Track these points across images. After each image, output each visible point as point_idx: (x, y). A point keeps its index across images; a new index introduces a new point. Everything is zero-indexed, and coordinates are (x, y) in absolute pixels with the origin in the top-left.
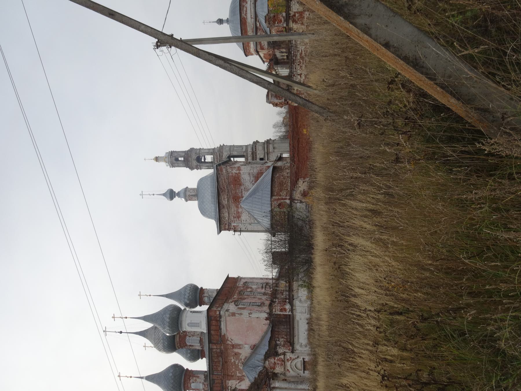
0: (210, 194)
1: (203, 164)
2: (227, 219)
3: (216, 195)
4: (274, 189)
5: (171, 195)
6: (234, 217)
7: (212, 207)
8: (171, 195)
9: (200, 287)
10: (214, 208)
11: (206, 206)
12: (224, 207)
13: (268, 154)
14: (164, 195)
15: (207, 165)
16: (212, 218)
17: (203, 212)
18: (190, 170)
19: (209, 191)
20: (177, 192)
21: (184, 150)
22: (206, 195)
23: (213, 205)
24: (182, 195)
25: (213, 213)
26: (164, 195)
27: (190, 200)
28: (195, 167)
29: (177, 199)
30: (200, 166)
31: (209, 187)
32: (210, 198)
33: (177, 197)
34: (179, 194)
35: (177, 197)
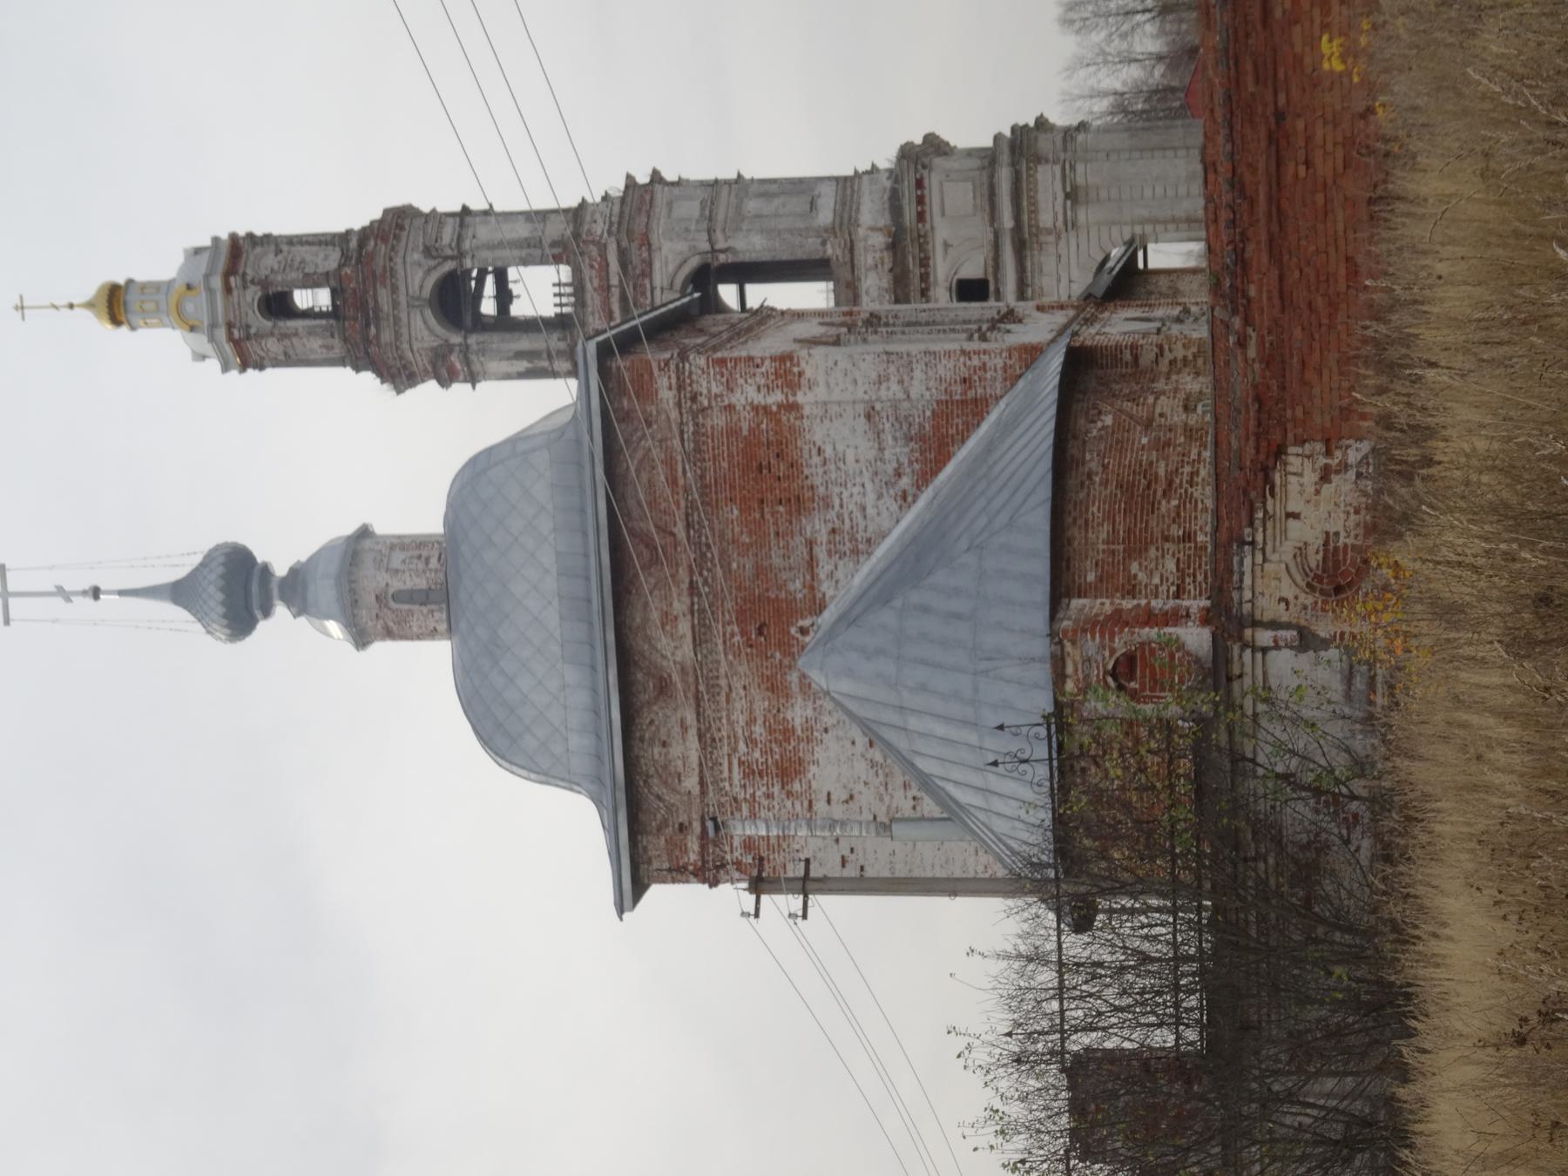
0: (550, 584)
1: (495, 340)
2: (691, 783)
4: (642, 817)
5: (236, 591)
6: (750, 772)
8: (236, 591)
9: (259, 560)
10: (581, 698)
12: (664, 688)
13: (1020, 247)
14: (180, 592)
15: (525, 343)
16: (567, 781)
17: (500, 728)
18: (386, 390)
19: (547, 558)
20: (280, 570)
23: (572, 675)
24: (324, 590)
25: (579, 742)
26: (180, 592)
27: (389, 634)
28: (421, 362)
29: (280, 627)
30: (465, 350)
31: (545, 525)
32: (552, 617)
33: (281, 611)
34: (296, 588)
35: (281, 611)
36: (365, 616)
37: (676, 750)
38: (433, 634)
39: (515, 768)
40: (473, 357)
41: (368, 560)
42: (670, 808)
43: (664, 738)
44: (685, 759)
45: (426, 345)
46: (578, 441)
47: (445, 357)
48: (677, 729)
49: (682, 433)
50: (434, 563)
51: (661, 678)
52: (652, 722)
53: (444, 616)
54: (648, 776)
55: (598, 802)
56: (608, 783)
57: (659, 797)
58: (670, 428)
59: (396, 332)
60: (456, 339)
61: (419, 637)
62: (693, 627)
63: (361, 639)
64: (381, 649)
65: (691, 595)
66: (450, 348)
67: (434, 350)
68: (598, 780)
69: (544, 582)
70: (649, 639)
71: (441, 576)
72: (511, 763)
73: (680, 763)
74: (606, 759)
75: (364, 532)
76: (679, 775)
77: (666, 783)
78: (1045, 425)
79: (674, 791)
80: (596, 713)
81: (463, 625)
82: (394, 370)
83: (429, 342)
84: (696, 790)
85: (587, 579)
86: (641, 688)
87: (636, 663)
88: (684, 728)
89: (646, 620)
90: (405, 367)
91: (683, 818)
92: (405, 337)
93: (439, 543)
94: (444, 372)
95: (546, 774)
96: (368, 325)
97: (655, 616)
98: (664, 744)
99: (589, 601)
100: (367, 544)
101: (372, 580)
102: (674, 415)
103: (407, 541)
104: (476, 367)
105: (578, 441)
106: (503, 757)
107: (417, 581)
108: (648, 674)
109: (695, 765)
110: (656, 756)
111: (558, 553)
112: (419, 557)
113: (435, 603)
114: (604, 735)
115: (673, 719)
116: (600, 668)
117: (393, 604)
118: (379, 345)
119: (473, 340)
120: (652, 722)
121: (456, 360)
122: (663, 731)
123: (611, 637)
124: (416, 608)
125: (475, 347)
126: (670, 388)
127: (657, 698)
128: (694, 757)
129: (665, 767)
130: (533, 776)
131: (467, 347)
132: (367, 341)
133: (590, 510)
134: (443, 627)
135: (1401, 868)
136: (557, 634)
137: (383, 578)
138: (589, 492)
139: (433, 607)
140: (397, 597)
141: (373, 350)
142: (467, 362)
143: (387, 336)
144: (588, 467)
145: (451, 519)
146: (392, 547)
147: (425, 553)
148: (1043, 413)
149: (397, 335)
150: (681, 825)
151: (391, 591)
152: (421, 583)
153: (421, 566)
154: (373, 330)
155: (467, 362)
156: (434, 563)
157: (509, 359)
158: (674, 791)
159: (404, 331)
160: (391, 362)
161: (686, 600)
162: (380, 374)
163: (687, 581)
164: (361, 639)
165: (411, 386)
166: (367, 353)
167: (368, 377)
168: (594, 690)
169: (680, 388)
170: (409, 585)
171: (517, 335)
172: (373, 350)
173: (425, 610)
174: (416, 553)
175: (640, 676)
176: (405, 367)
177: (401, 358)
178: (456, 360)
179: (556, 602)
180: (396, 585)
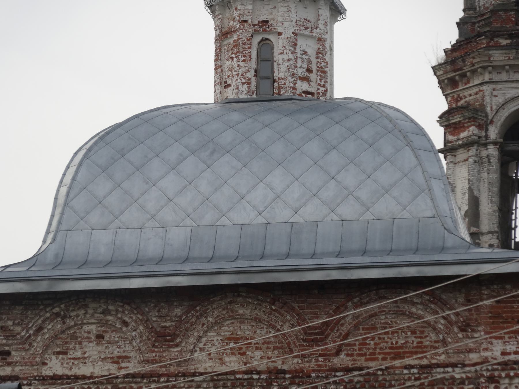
0: (282, 214)
1: (491, 176)
3: (276, 266)
4: (17, 311)
7: (169, 228)
10: (152, 246)
11: (170, 183)
12: (164, 338)
15: (488, 208)
16: (57, 230)
17: (121, 151)
18: (438, 56)
19: (311, 212)
21: (366, 99)
22: (277, 179)
23: (178, 236)
25: (102, 243)
27: (223, 35)
28: (469, 94)
30: (481, 143)
31: (348, 210)
32: (243, 215)
37: (92, 350)
38: (222, 83)
39: (72, 170)
40: (473, 151)
42: (27, 341)
43: (107, 337)
44: (83, 359)
45: (487, 99)
46: (443, 249)
47: (473, 120)
48: (116, 353)
49: (454, 365)
50: (305, 86)
51: (174, 336)
52: (125, 324)
53: (243, 96)
54: (64, 318)
55: (34, 261)
56: (57, 273)
57: (40, 329)
58: (459, 352)
59: (503, 67)
60: (493, 133)
61: (218, 68)
62: (233, 373)
65: (269, 371)
66: (484, 126)
67: (483, 107)
68: (59, 264)
69: (285, 207)
70: (219, 323)
72: (80, 165)
73: (78, 354)
74: (83, 271)
76: (65, 353)
77: (56, 337)
79: (46, 348)
80: (135, 262)
81: (235, 116)
82: (460, 63)
83: (491, 104)
84: (46, 372)
85: (288, 256)
86: (164, 312)
87: (194, 307)
88: (117, 360)
89: (242, 320)
90: (463, 76)
91: (16, 356)
92: (496, 77)
93: (325, 93)
94: (456, 119)
95: (66, 204)
96: (510, 36)
97: (245, 330)
98: (100, 337)
99: (262, 257)
100: (325, 12)
102: (474, 357)
103: (327, 57)
104: (462, 155)
105: (443, 249)
106: (85, 157)
108: (180, 321)
109: (76, 371)
110: (86, 328)
111: (316, 224)
112: (309, 70)
113: (257, 87)
114: (112, 270)
115: (128, 348)
116: (188, 267)
117: (257, 39)
118: (488, 48)
119: (492, 151)
120: (125, 324)
121: (471, 132)
122: (115, 336)
123: (224, 280)
124: (253, 65)
125: (484, 153)
126: (504, 353)
127: (152, 330)
128: (85, 370)
129: (74, 337)
130: (64, 190)
131: (485, 145)
132: (493, 35)
133: (367, 260)
134: (230, 94)
136: (224, 221)
138: (389, 259)
139: (253, 84)
141: (484, 41)
142: (467, 145)
143: (498, 57)
144: (417, 258)
145: (355, 108)
146: (320, 40)
147: (313, 76)
149: (499, 69)
150: (8, 353)
151: (271, 37)
152: (281, 71)
153: (300, 72)
154: (504, 42)
155: (467, 145)
156: (305, 86)
157: (470, 190)
158: (46, 348)
159: (504, 76)
160: (469, 61)
161: (263, 365)
162: (456, 48)
163: (285, 367)
165: (441, 83)
166: (479, 35)
167: (452, 36)
168: (161, 260)
169: (505, 365)
170: (278, 58)
171: (496, 199)
172: (484, 41)
173: (251, 75)
174: (314, 67)
175: (178, 311)
176: (463, 76)
177: (474, 72)
178: (471, 132)
179: (260, 220)
180: (279, 44)
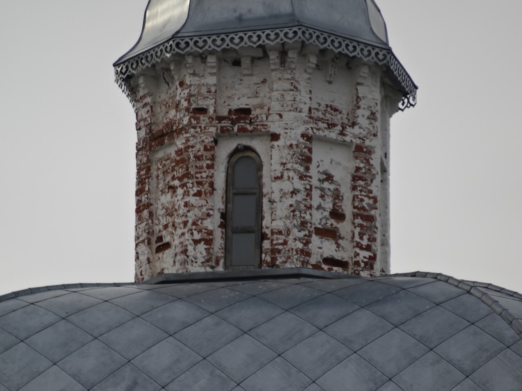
27: (153, 139)
36: (201, 81)
38: (152, 241)
41: (334, 94)
50: (326, 248)
53: (196, 269)
63: (138, 73)
64: (119, 122)
71: (293, 265)
75: (397, 88)
78: (163, 12)
81: (180, 311)
100: (371, 93)
101: (286, 103)
103: (375, 187)
107: (282, 208)
112: (337, 215)
124: (218, 202)
134: (168, 264)
135: (167, 205)
137: (291, 127)
139: (218, 242)
140: (244, 159)
146: (361, 151)
147: (345, 228)
148: (163, 12)
150: (208, 92)
151: (259, 145)
152: (276, 217)
153: (317, 218)
156: (326, 248)
164: (138, 73)
170: (271, 188)
173: (213, 224)
174: (347, 209)
180: (273, 158)
